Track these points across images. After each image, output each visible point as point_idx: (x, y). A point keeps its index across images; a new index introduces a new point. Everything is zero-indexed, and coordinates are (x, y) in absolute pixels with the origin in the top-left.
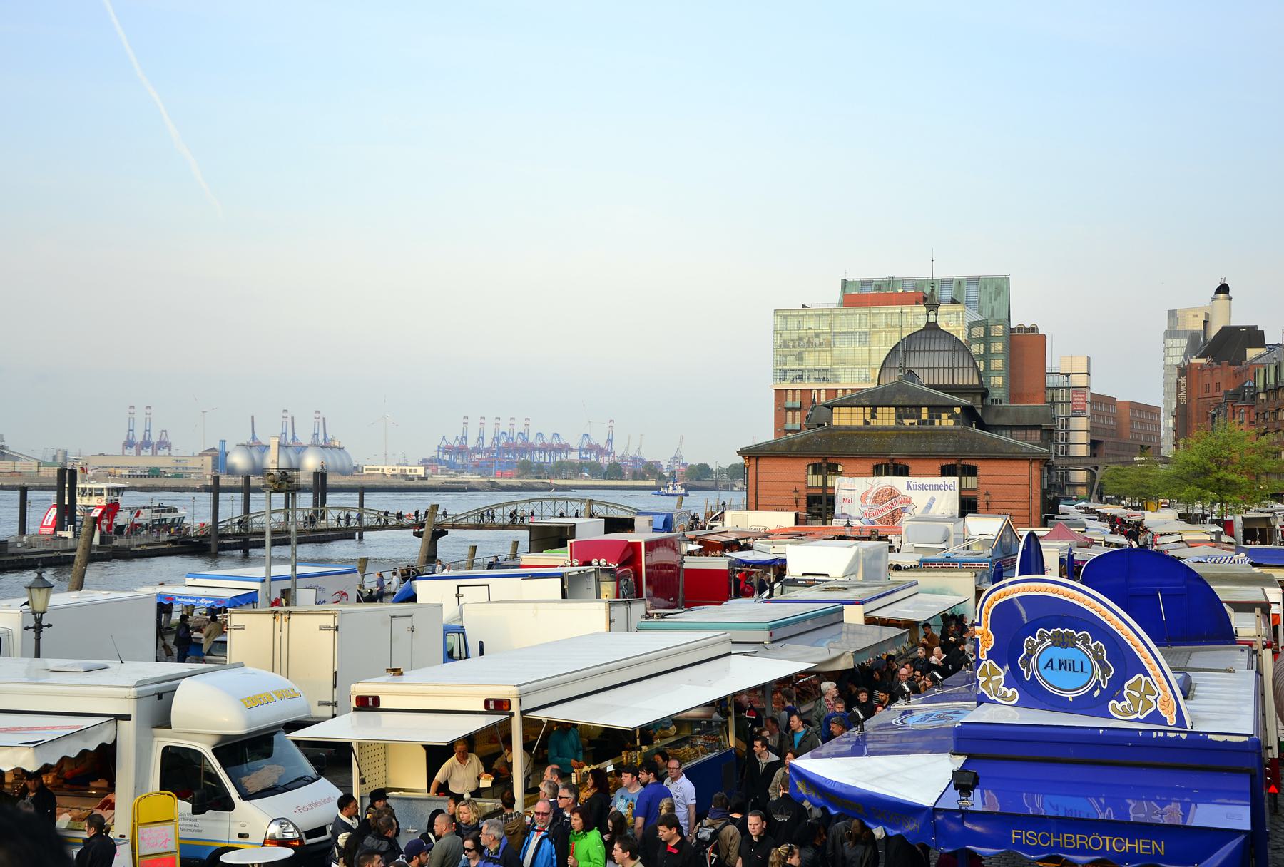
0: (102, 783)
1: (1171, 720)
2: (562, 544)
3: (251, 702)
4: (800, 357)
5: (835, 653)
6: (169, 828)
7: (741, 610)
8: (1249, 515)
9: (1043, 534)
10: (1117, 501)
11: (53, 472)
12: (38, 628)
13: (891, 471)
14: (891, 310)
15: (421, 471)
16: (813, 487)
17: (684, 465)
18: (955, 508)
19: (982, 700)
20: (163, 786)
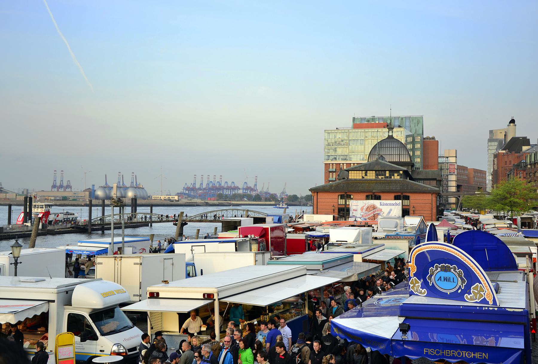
0: (43, 329)
1: (491, 302)
2: (235, 228)
3: (105, 295)
4: (335, 150)
5: (350, 274)
6: (71, 348)
7: (310, 256)
8: (523, 216)
9: (437, 224)
10: (468, 210)
11: (22, 198)
12: (16, 264)
15: (176, 198)
16: (340, 205)
17: (287, 195)
18: (400, 213)
19: (411, 294)
20: (68, 330)
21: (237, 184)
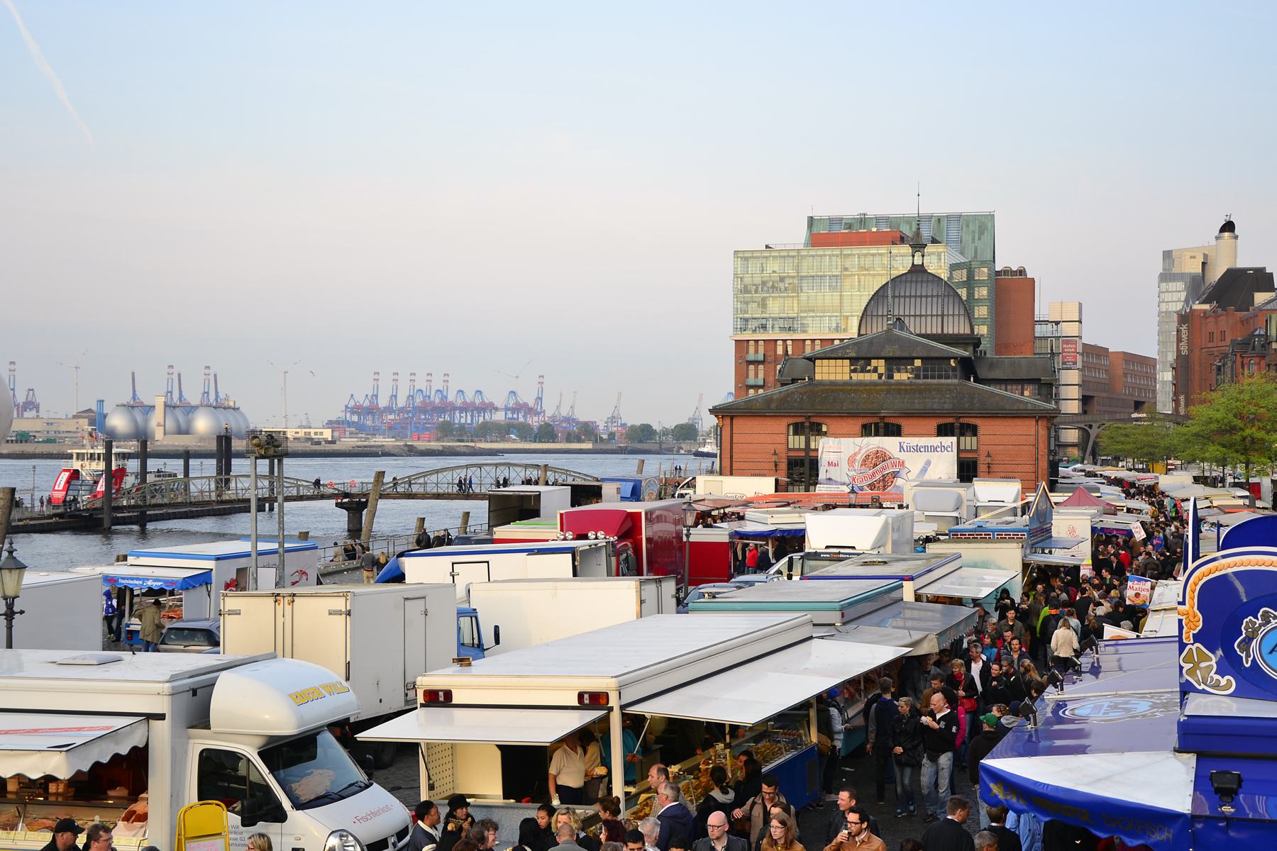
0: (120, 792)
2: (534, 513)
3: (301, 698)
4: (763, 304)
5: (917, 636)
7: (771, 585)
9: (1060, 500)
12: (10, 615)
13: (881, 431)
14: (865, 251)
15: (327, 434)
16: (794, 450)
17: (623, 425)
20: (202, 795)
21: (489, 397)
